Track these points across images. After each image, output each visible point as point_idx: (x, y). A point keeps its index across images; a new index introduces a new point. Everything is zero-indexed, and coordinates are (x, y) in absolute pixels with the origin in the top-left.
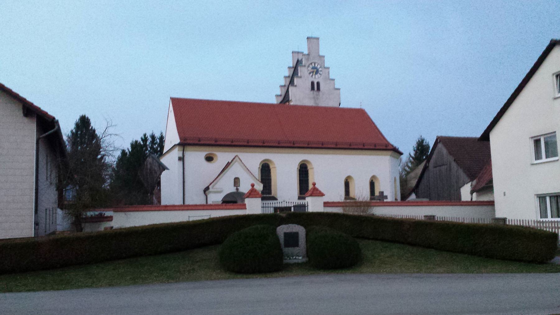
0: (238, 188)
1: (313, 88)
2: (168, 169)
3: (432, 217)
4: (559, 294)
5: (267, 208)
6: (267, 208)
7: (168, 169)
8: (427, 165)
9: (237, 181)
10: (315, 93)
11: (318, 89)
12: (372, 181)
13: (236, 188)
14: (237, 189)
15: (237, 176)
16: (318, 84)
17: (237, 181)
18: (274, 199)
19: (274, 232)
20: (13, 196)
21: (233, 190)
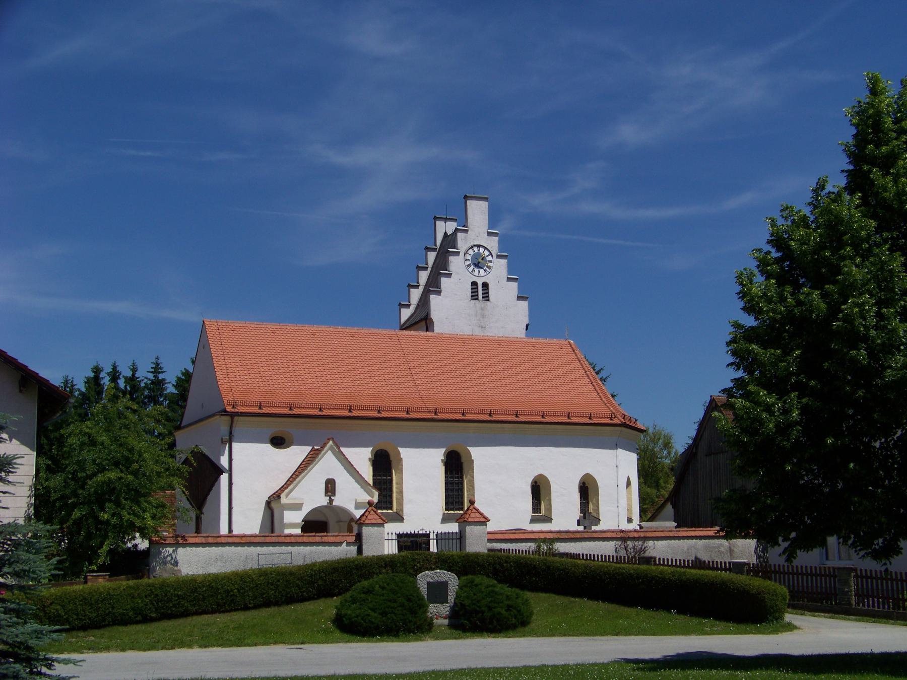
0: (332, 498)
1: (474, 296)
2: (741, 309)
3: (653, 560)
4: (731, 679)
5: (451, 541)
6: (451, 541)
7: (741, 309)
8: (694, 450)
9: (330, 487)
10: (479, 304)
11: (486, 297)
12: (584, 483)
13: (328, 498)
14: (331, 501)
15: (331, 477)
16: (485, 285)
17: (330, 487)
18: (399, 518)
19: (414, 583)
20: (452, 539)
21: (323, 501)
